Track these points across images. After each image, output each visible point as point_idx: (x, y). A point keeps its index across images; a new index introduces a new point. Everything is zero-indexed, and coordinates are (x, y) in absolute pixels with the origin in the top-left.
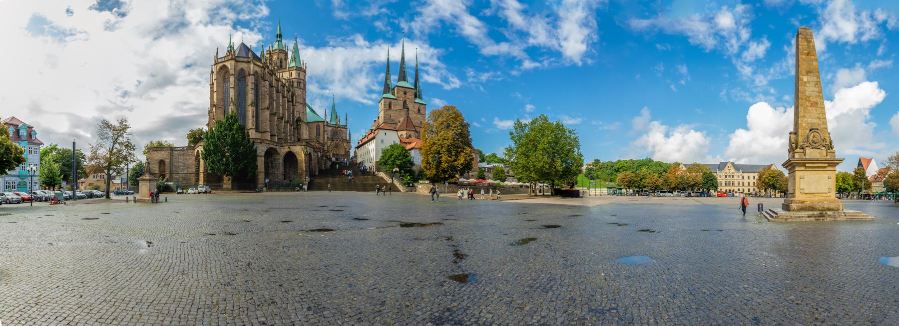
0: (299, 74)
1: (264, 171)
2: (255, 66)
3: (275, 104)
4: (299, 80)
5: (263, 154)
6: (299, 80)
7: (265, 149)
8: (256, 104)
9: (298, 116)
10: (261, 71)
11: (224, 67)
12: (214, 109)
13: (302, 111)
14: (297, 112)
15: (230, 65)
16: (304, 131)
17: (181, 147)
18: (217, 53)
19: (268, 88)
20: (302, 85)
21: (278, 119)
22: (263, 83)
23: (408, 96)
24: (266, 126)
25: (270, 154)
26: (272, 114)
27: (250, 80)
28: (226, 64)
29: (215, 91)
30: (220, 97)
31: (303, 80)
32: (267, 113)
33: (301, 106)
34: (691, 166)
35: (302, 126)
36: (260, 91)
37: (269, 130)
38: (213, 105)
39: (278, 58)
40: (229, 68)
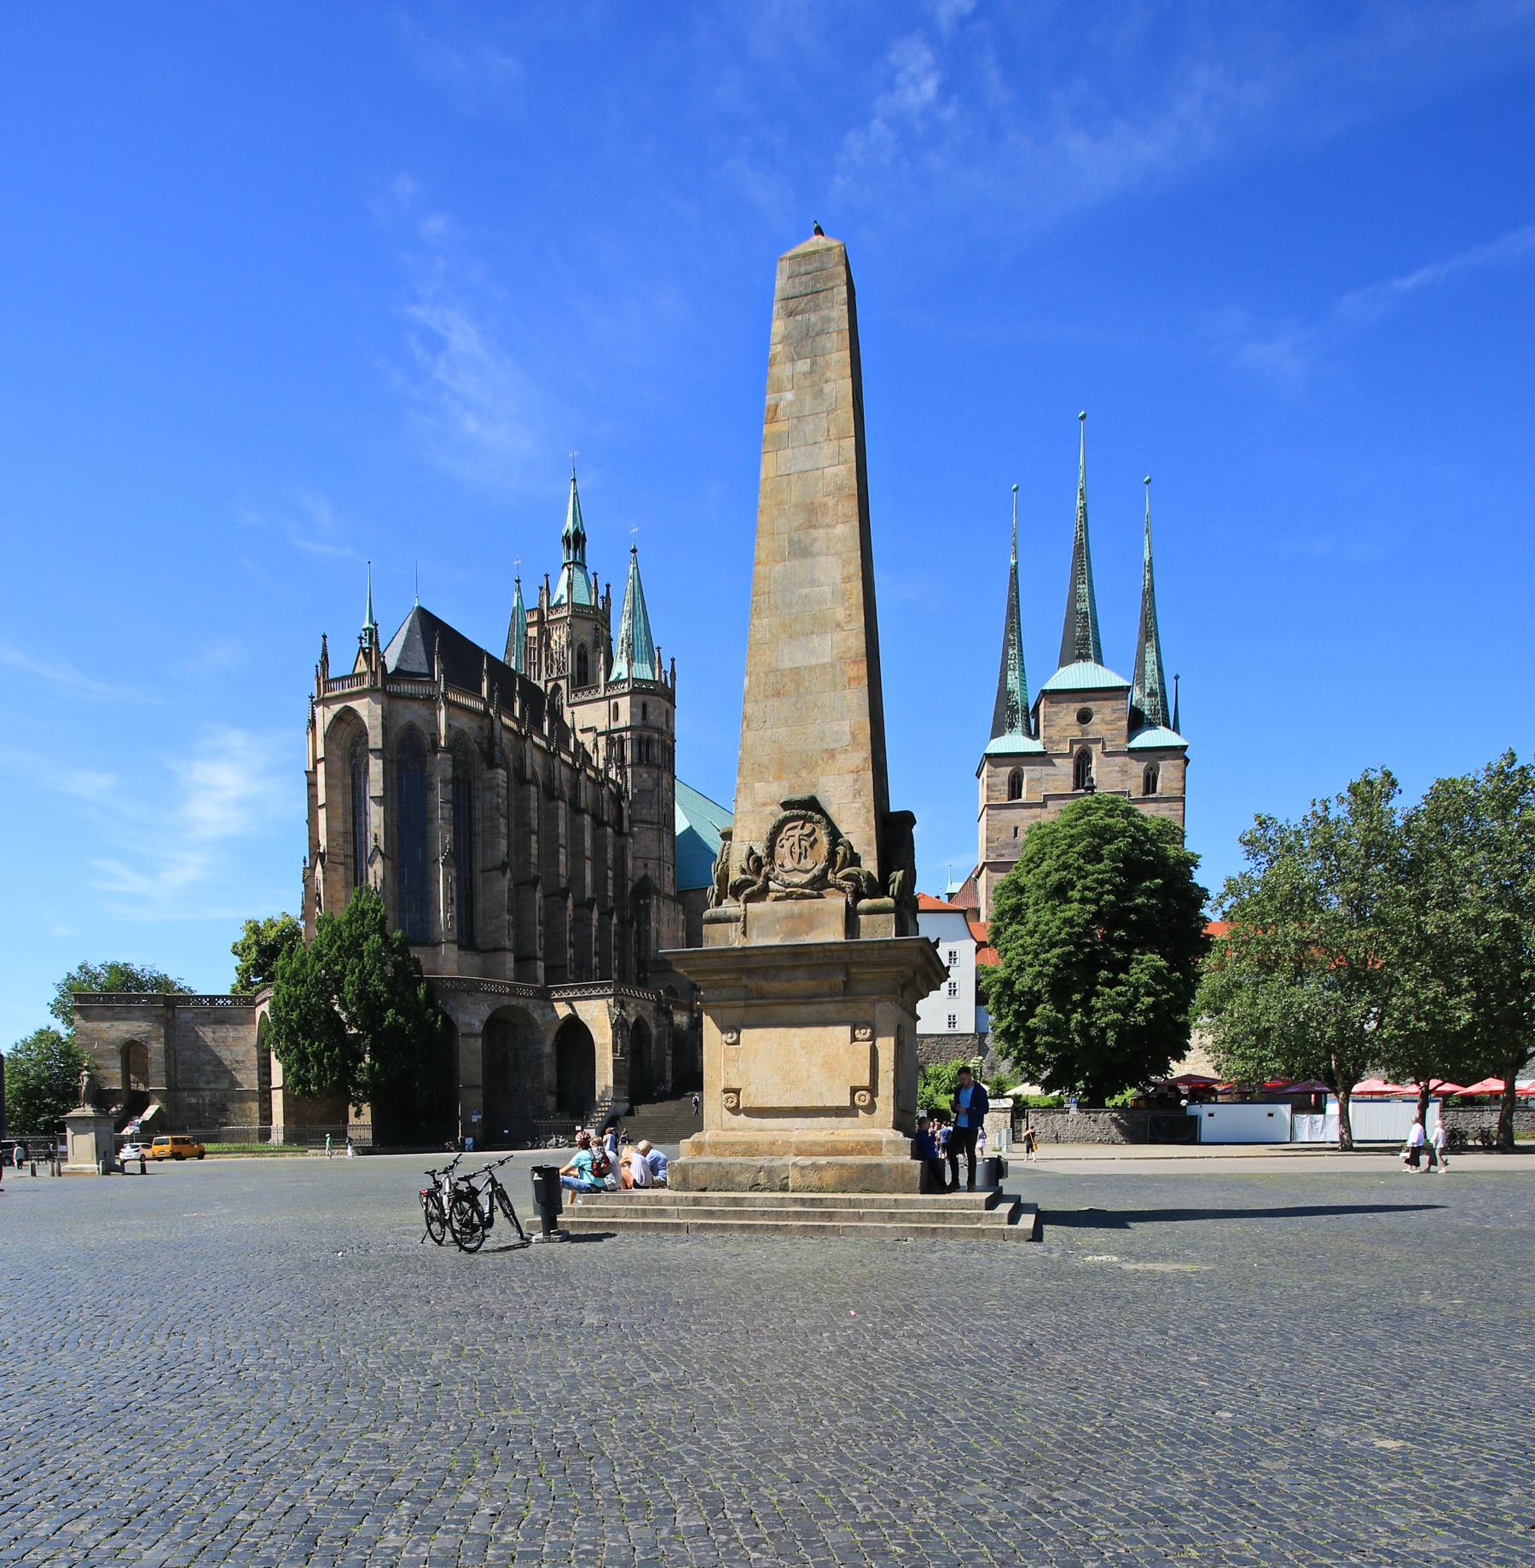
0: (644, 706)
1: (479, 1082)
2: (457, 713)
3: (534, 845)
4: (645, 734)
5: (478, 1026)
6: (645, 734)
7: (485, 1012)
8: (462, 857)
9: (641, 873)
10: (481, 728)
11: (346, 718)
12: (319, 868)
13: (655, 855)
14: (635, 858)
15: (368, 711)
16: (664, 930)
17: (1005, 654)
18: (325, 655)
19: (503, 792)
20: (656, 751)
21: (546, 897)
22: (487, 775)
23: (1096, 727)
24: (498, 925)
25: (500, 1026)
26: (523, 885)
27: (441, 768)
28: (353, 704)
29: (320, 803)
30: (339, 826)
31: (660, 731)
32: (504, 884)
33: (652, 835)
34: (124, 1015)
35: (654, 909)
36: (478, 804)
37: (508, 944)
38: (315, 854)
39: (570, 644)
40: (366, 720)
